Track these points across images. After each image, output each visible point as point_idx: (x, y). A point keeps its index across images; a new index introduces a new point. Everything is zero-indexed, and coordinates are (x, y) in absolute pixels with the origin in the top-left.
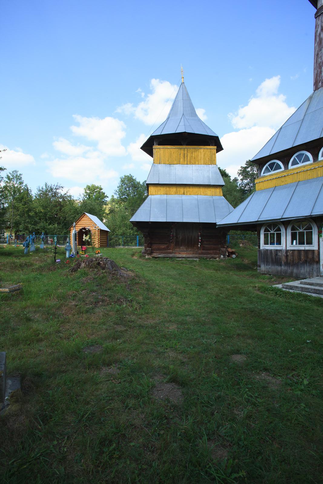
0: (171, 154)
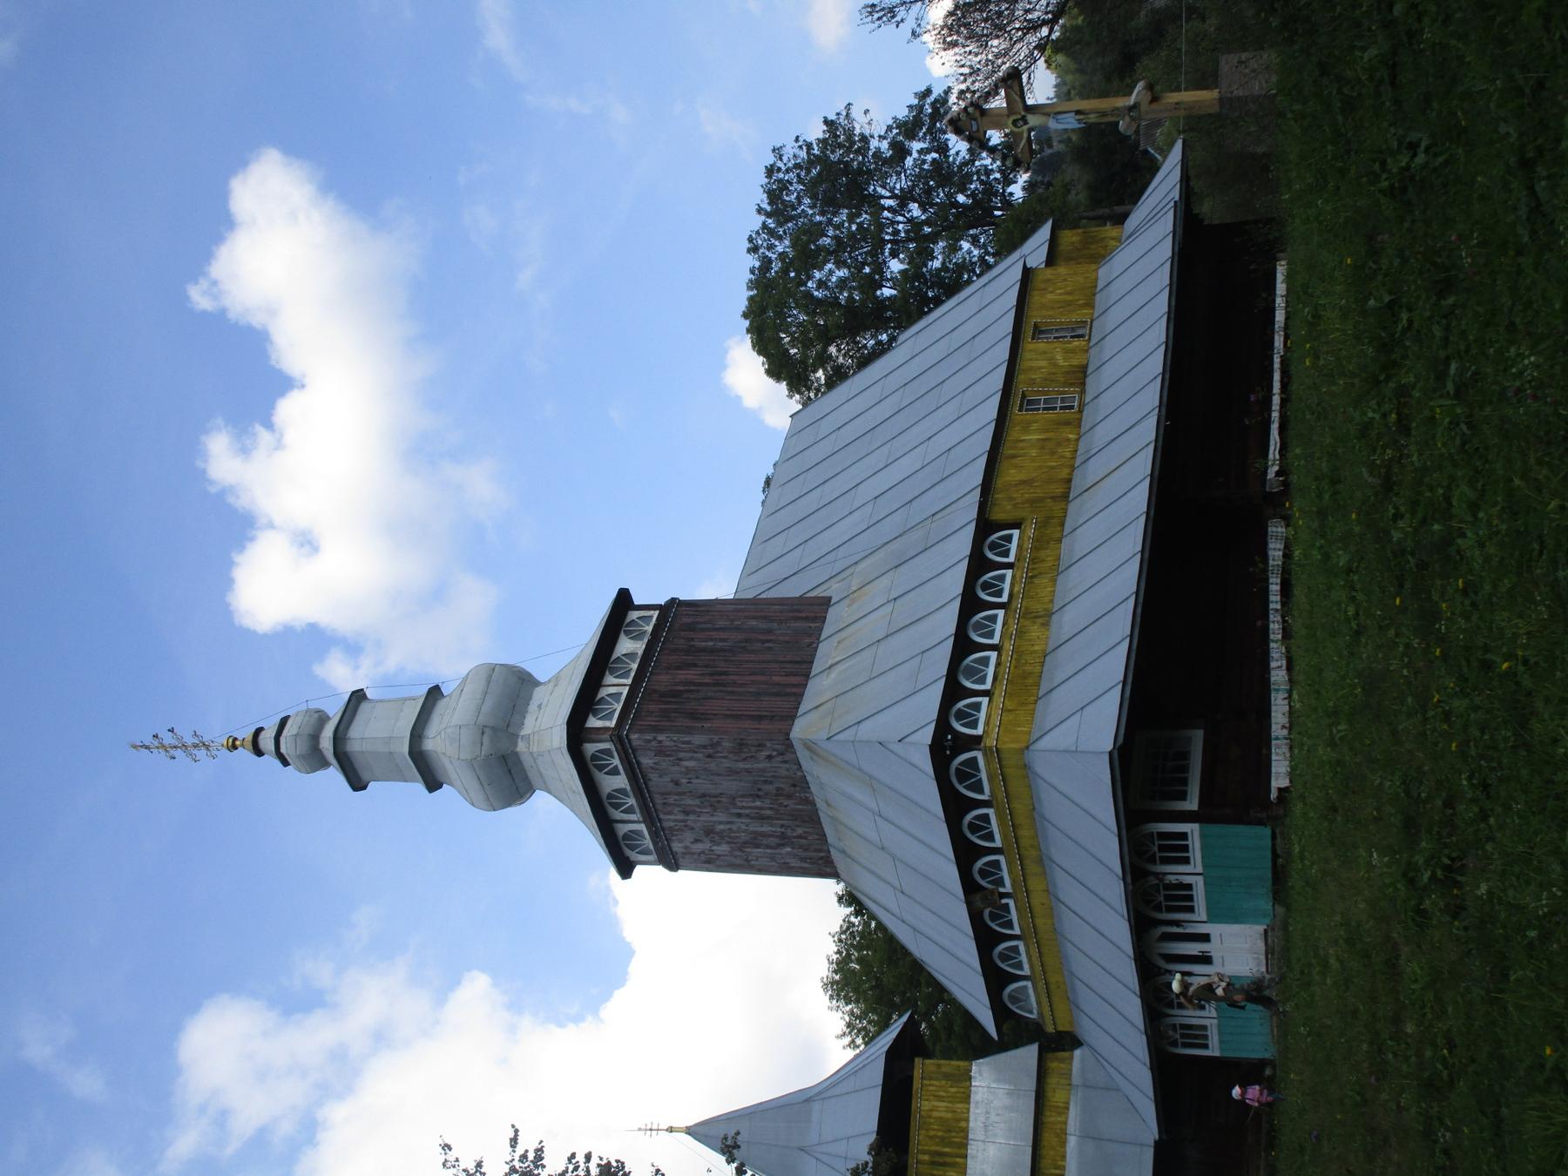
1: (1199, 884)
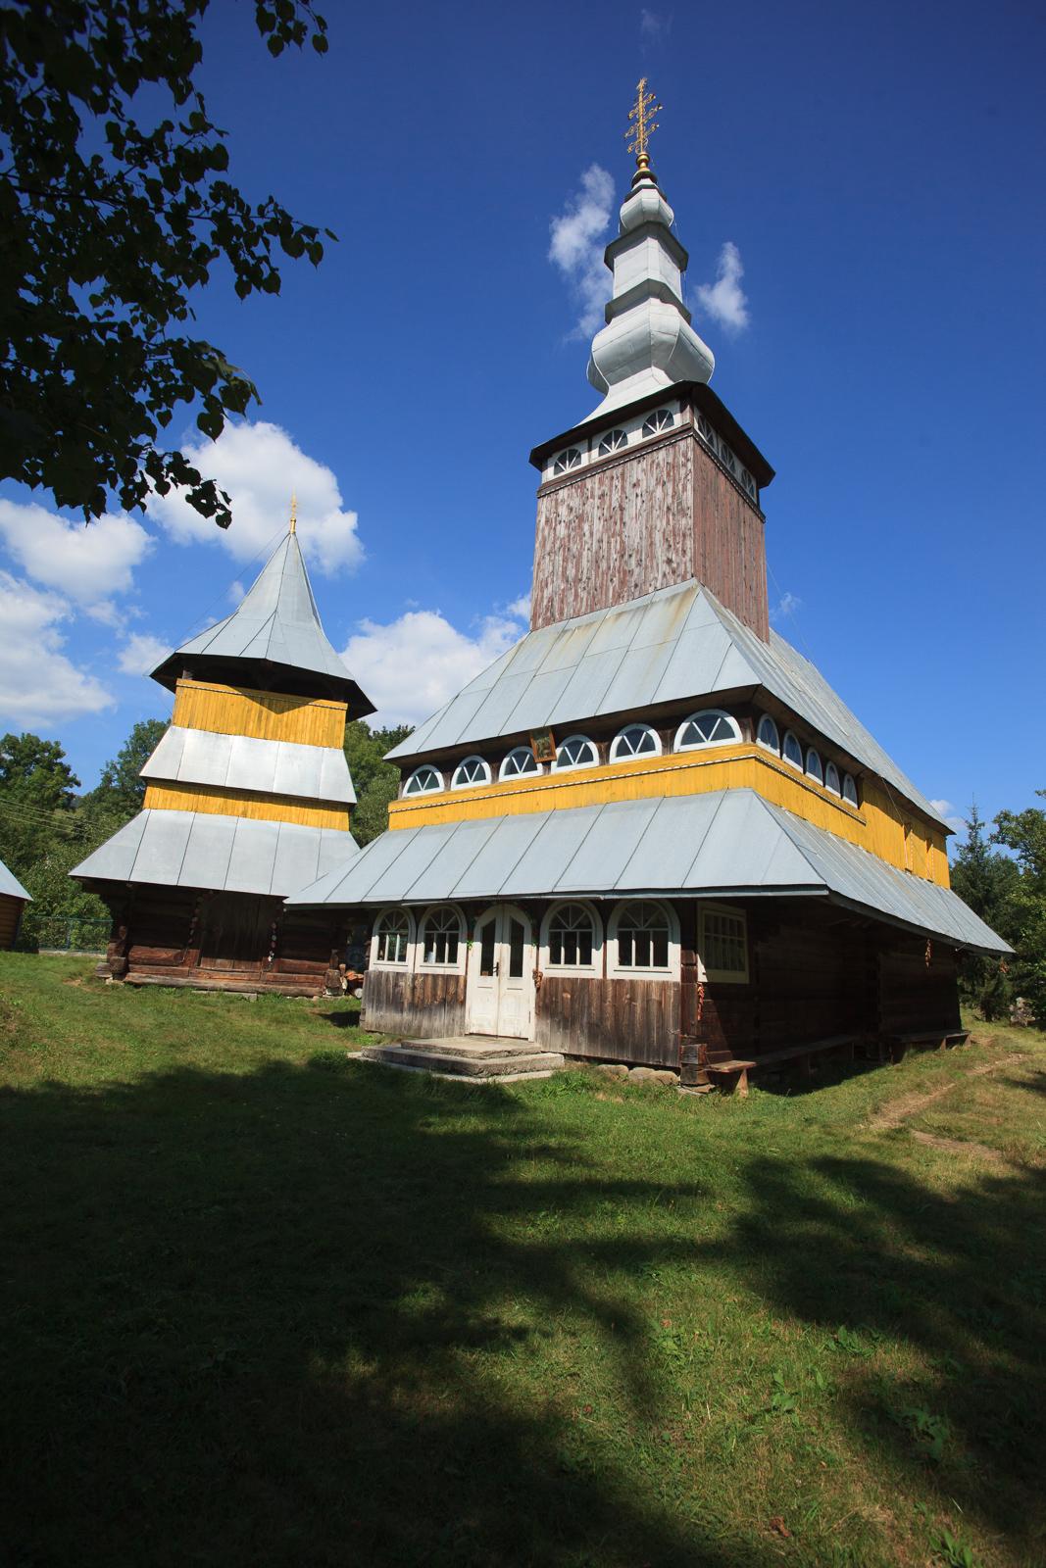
0: (224, 707)
1: (592, 972)
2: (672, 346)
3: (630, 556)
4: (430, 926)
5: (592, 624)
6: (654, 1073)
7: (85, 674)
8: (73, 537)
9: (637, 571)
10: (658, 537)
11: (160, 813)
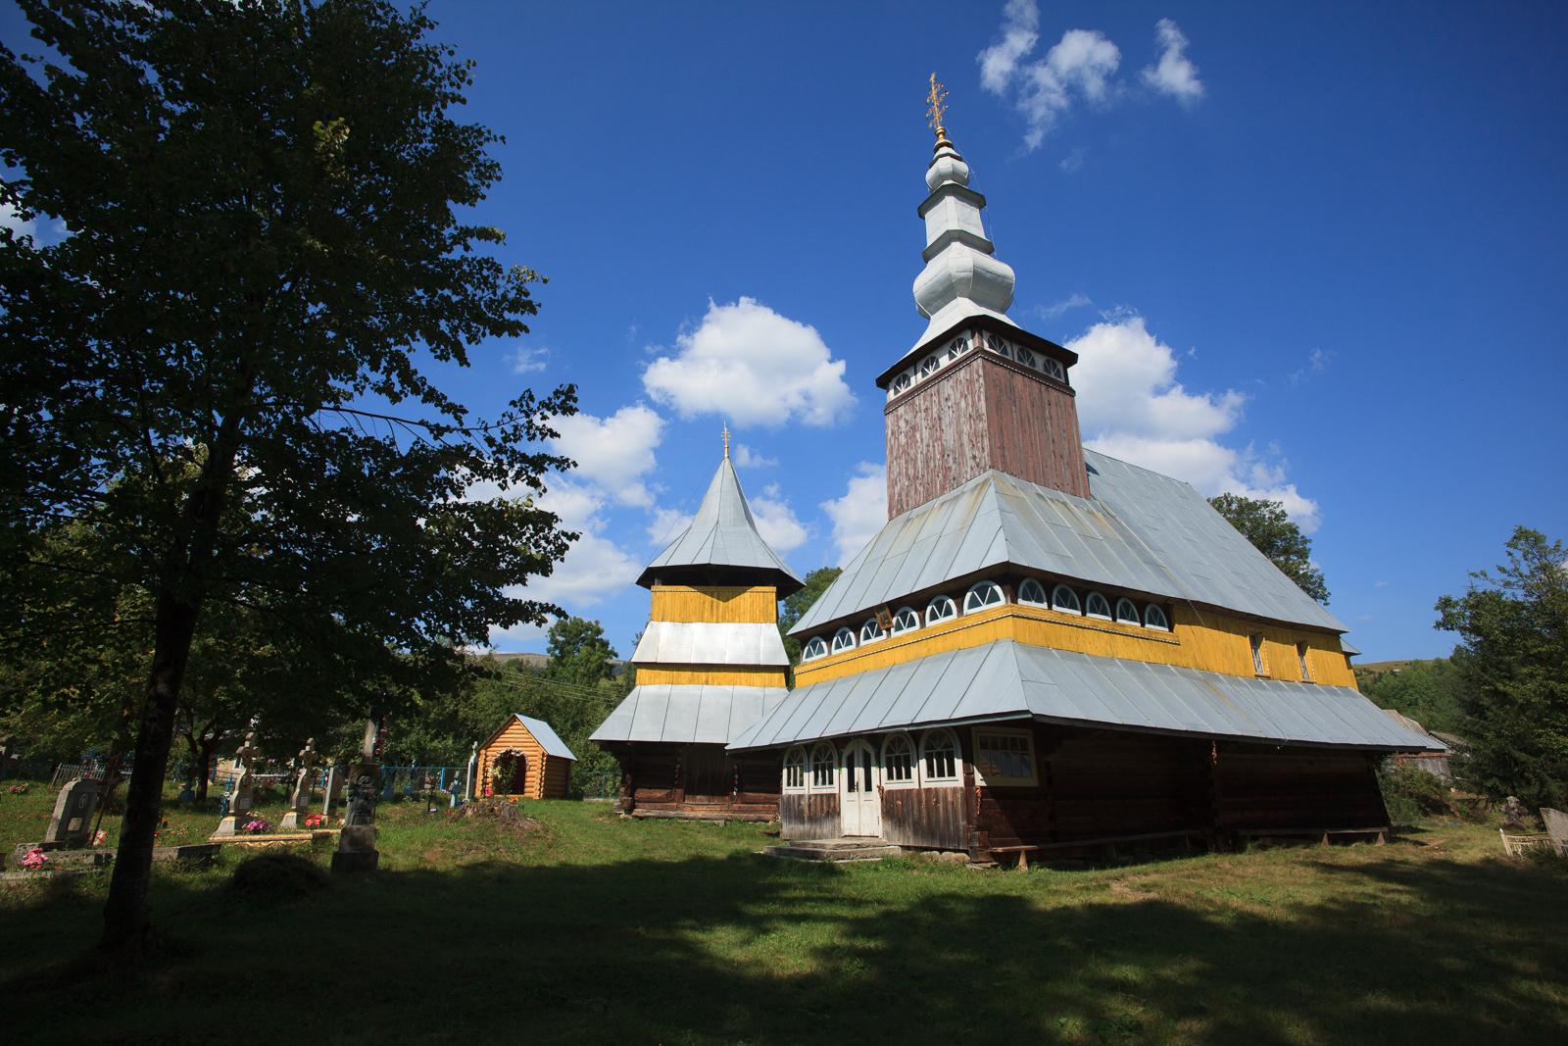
0: (685, 603)
1: (911, 784)
2: (970, 279)
3: (948, 455)
4: (816, 759)
5: (925, 513)
6: (954, 855)
7: (628, 553)
8: (604, 432)
9: (954, 467)
10: (965, 438)
11: (648, 688)
